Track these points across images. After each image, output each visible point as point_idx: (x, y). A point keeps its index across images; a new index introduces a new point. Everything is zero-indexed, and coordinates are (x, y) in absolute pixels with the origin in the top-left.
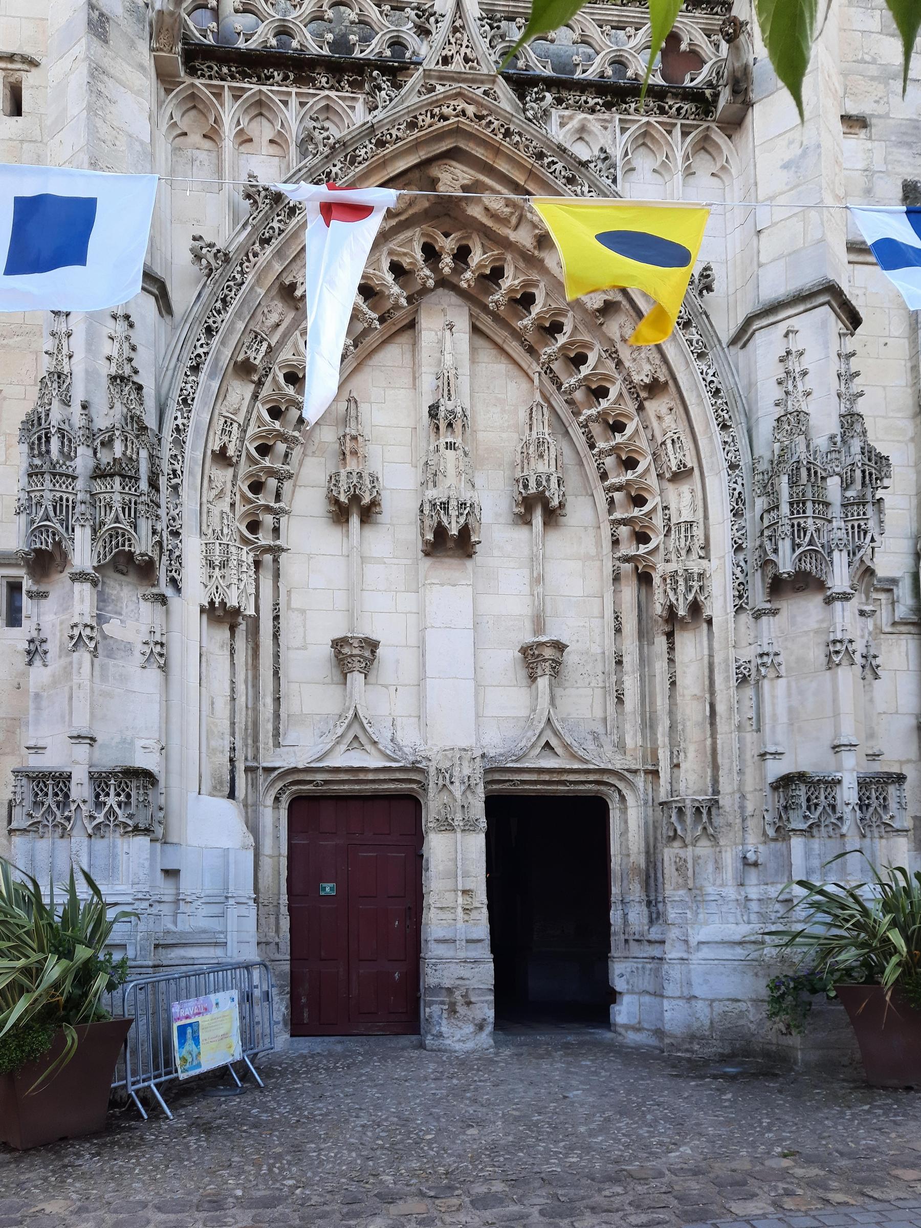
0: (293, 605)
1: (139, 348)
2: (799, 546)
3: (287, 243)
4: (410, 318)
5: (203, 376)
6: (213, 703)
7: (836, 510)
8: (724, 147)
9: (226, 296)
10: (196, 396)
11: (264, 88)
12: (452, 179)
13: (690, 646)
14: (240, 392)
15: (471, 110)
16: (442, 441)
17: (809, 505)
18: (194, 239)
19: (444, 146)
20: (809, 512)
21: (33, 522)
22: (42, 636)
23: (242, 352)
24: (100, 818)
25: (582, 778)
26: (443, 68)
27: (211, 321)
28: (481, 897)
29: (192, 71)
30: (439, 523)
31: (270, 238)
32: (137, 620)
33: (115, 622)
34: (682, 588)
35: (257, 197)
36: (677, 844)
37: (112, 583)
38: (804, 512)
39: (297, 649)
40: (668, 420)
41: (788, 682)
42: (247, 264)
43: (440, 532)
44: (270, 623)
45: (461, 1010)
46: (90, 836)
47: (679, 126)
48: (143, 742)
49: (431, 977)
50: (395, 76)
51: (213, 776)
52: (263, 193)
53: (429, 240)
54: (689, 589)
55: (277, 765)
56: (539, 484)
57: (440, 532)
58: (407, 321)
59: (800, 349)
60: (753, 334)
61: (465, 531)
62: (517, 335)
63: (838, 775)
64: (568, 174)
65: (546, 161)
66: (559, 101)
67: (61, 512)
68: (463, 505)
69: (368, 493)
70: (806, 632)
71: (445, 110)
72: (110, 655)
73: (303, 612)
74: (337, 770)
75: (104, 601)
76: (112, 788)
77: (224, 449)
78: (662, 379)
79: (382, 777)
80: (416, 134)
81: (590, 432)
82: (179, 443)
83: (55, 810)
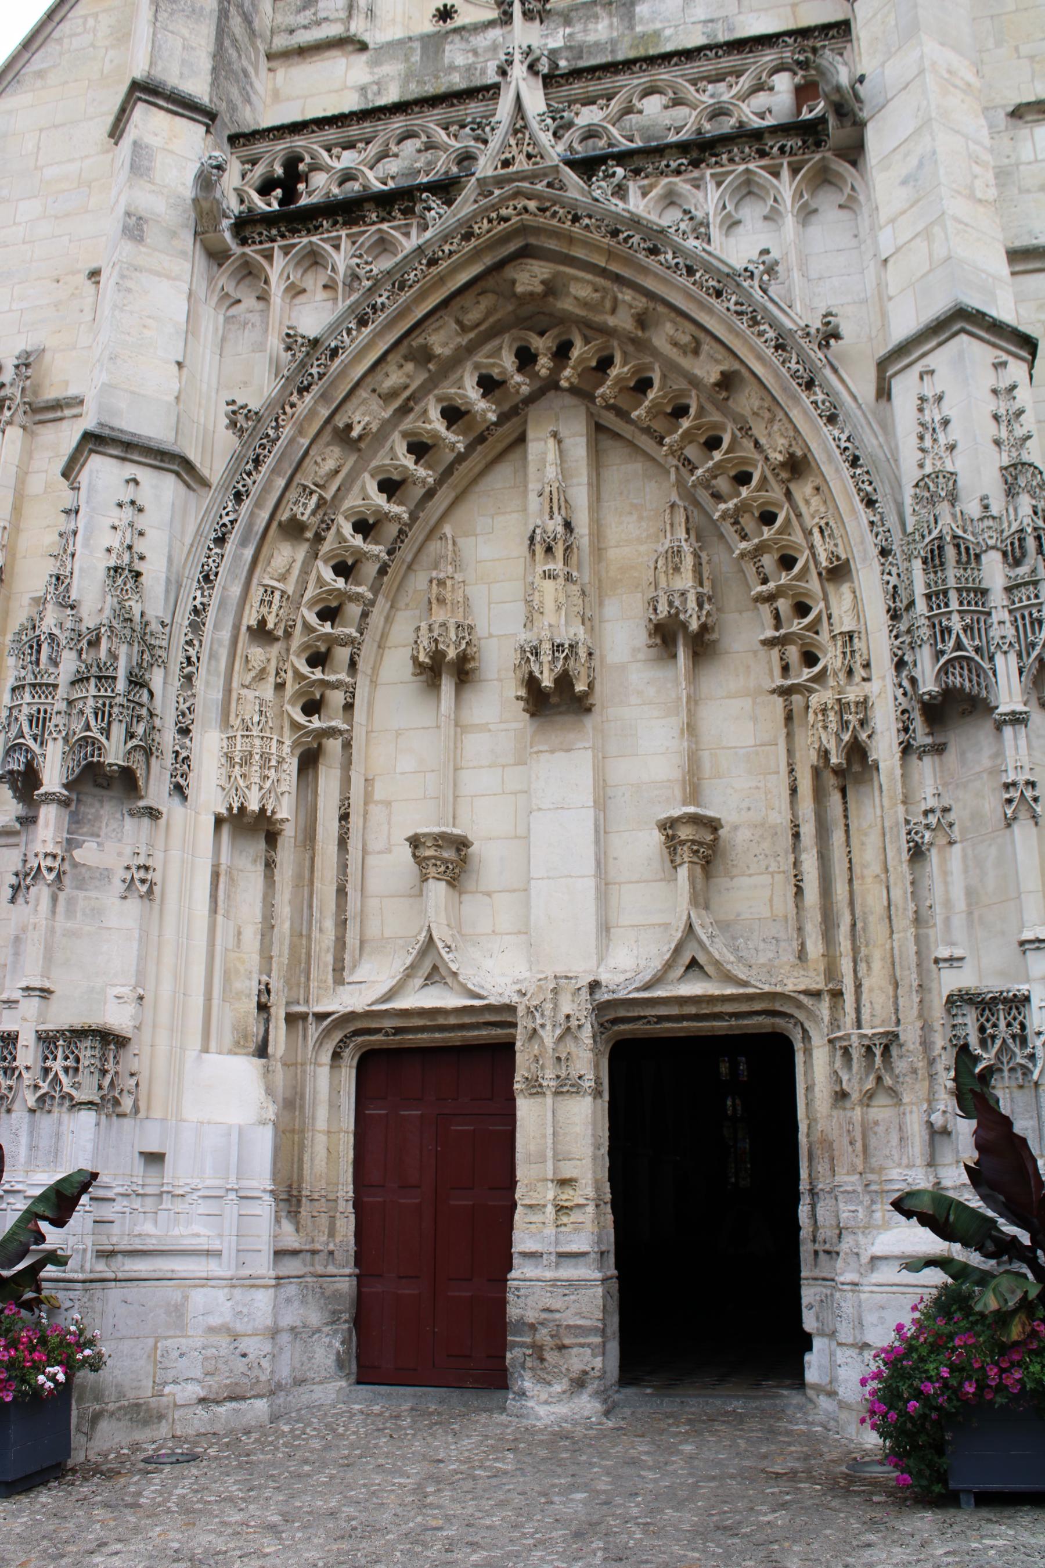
0: (378, 795)
1: (148, 532)
2: (943, 652)
4: (520, 431)
5: (230, 546)
6: (239, 933)
7: (997, 598)
8: (846, 174)
10: (220, 569)
11: (314, 239)
12: (530, 277)
14: (286, 555)
15: (532, 205)
16: (539, 570)
17: (953, 595)
18: (228, 404)
19: (512, 247)
20: (954, 605)
24: (45, 1087)
25: (744, 1008)
26: (502, 172)
30: (531, 673)
31: (310, 385)
32: (120, 840)
33: (90, 845)
37: (90, 800)
38: (947, 605)
39: (379, 853)
41: (964, 849)
43: (532, 683)
44: (335, 825)
45: (551, 1357)
46: (32, 1111)
47: (785, 165)
48: (117, 991)
49: (513, 1312)
50: (448, 193)
51: (235, 1028)
54: (844, 725)
56: (671, 604)
57: (532, 683)
59: (938, 391)
61: (564, 681)
63: (1024, 988)
64: (649, 244)
66: (637, 172)
68: (558, 647)
69: (452, 647)
70: (978, 773)
71: (503, 212)
72: (81, 885)
73: (388, 804)
75: (77, 822)
76: (60, 1050)
77: (262, 622)
79: (467, 1020)
81: (743, 529)
82: (196, 627)
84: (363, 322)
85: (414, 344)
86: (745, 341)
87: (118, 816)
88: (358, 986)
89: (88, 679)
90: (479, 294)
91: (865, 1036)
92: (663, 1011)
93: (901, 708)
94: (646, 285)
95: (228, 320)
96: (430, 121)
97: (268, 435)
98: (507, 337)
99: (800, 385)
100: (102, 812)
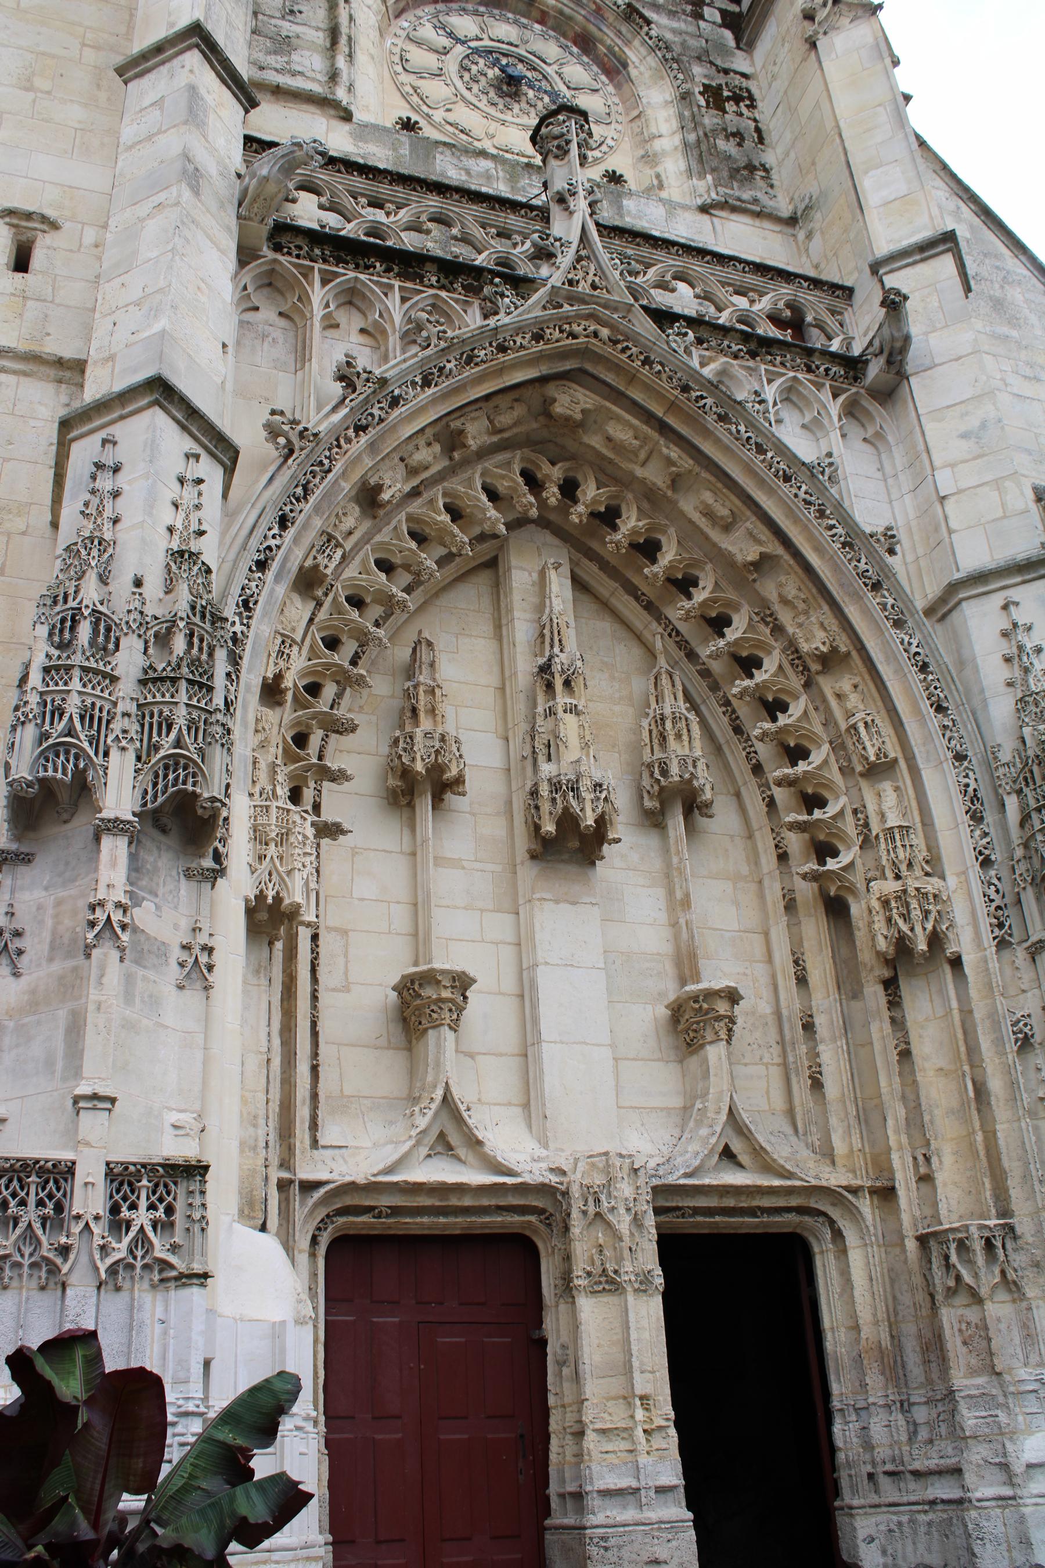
3: (382, 437)
4: (493, 554)
5: (270, 575)
8: (874, 413)
9: (308, 482)
11: (362, 277)
12: (572, 401)
13: (925, 1006)
15: (605, 332)
19: (568, 365)
21: (46, 736)
22: (17, 925)
23: (311, 557)
25: (781, 1203)
27: (287, 508)
28: (665, 1409)
29: (277, 248)
30: (566, 810)
34: (916, 914)
35: (355, 379)
36: (961, 1299)
39: (334, 990)
40: (853, 700)
42: (336, 450)
48: (174, 1117)
52: (364, 376)
53: (529, 466)
55: (323, 1176)
58: (488, 557)
60: (959, 603)
62: (633, 591)
65: (694, 394)
66: (700, 341)
67: (91, 726)
71: (575, 328)
73: (344, 932)
74: (417, 1188)
78: (843, 649)
79: (485, 1202)
80: (541, 346)
81: (734, 711)
83: (39, 1232)
84: (427, 383)
85: (452, 425)
86: (805, 529)
87: (174, 873)
88: (337, 1151)
89: (174, 680)
90: (516, 400)
91: (986, 1226)
92: (702, 1202)
93: (994, 905)
94: (702, 448)
95: (242, 323)
96: (469, 214)
97: (321, 463)
98: (518, 453)
99: (866, 585)
100: (160, 864)
